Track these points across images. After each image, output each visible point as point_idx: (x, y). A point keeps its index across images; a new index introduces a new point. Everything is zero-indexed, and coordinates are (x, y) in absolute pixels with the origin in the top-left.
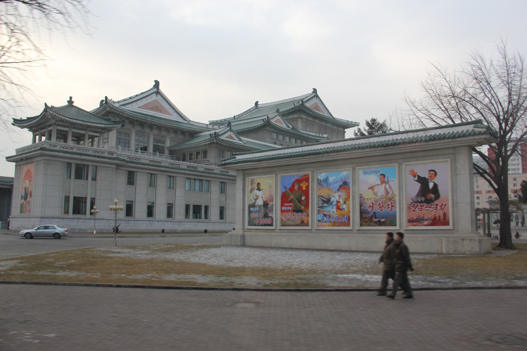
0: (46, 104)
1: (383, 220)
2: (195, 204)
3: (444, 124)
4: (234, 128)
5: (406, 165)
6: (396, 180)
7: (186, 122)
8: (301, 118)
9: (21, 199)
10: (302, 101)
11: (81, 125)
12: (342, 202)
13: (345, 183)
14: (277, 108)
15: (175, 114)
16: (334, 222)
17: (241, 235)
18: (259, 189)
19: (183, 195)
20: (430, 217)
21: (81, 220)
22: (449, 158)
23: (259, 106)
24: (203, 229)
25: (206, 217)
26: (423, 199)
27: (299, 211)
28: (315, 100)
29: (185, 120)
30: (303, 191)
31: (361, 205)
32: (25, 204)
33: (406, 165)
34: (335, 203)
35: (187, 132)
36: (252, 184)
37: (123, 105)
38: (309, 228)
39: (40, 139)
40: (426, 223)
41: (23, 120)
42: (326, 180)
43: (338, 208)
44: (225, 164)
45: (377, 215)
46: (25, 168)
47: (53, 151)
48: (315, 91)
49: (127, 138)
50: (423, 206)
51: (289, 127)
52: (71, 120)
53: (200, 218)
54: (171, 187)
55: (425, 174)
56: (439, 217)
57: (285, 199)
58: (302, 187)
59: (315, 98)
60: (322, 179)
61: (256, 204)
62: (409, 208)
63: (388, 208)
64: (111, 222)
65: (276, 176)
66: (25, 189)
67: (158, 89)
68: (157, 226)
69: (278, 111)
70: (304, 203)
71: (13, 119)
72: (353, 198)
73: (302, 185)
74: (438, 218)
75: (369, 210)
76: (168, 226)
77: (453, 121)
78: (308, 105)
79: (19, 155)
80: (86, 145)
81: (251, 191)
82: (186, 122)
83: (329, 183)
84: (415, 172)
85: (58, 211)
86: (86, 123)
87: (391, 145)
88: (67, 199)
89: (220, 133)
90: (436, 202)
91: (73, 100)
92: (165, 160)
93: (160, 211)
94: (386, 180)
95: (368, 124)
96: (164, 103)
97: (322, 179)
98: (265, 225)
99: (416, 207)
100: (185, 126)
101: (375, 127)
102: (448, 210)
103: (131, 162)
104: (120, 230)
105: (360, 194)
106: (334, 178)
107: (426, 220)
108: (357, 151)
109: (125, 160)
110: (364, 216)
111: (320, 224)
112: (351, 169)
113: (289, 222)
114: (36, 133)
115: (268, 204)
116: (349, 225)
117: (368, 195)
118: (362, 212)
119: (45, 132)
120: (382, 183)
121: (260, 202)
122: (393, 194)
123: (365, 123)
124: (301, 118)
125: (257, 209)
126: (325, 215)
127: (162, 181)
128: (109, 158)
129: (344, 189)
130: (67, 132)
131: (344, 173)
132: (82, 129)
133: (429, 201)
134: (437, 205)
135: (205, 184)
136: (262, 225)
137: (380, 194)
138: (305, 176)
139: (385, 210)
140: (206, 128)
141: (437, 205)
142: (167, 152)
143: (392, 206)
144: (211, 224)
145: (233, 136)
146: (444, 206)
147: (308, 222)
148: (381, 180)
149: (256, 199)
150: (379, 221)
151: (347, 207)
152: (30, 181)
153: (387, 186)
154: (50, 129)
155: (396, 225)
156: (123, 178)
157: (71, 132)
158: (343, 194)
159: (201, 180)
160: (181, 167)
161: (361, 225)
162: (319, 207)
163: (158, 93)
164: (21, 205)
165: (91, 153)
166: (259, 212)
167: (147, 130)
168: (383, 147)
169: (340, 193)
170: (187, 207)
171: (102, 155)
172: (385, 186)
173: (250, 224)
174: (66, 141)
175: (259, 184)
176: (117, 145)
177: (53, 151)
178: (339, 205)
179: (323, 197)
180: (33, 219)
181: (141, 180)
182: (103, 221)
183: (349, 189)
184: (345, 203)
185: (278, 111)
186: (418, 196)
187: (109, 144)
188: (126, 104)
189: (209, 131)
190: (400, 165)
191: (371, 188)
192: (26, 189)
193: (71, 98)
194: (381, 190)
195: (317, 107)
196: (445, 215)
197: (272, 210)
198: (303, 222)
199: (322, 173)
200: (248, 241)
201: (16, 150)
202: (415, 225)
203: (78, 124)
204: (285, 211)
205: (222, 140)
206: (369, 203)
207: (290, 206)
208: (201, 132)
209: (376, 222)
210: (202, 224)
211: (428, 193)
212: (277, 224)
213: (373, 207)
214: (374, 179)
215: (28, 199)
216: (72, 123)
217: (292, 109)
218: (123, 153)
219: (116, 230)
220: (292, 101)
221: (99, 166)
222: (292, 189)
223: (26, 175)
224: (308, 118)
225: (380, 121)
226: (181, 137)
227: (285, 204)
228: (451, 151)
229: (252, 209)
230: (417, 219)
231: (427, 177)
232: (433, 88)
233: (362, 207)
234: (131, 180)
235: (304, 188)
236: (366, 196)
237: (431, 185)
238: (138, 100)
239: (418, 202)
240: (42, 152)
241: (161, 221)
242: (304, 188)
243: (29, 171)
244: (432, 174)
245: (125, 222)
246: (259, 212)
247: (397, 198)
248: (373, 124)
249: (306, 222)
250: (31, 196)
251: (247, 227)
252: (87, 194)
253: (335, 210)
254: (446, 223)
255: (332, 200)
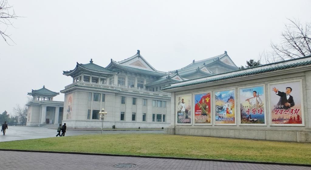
0: (77, 63)
1: (256, 120)
2: (158, 114)
3: (296, 57)
4: (180, 75)
5: (271, 85)
6: (264, 95)
7: (155, 71)
8: (218, 68)
9: (67, 112)
10: (218, 58)
11: (97, 73)
12: (230, 109)
13: (232, 98)
14: (204, 63)
15: (149, 67)
16: (226, 121)
17: (173, 129)
18: (183, 103)
19: (151, 109)
20: (288, 117)
21: (96, 122)
22: (301, 79)
23: (195, 63)
24: (161, 127)
25: (164, 121)
26: (283, 106)
27: (204, 114)
28: (226, 58)
29: (154, 70)
30: (207, 103)
31: (241, 111)
32: (68, 114)
33: (271, 85)
34: (226, 109)
35: (157, 77)
36: (179, 100)
37: (121, 63)
38: (211, 124)
39: (77, 81)
40: (285, 122)
41: (68, 72)
42: (220, 96)
43: (227, 112)
44: (164, 89)
45: (251, 116)
46: (69, 96)
47: (82, 86)
48: (226, 52)
49: (123, 80)
50: (282, 111)
51: (211, 73)
52: (91, 71)
53: (161, 121)
54: (145, 105)
55: (283, 90)
56: (294, 118)
57: (197, 108)
58: (206, 100)
59: (226, 56)
60: (218, 96)
61: (182, 111)
62: (272, 112)
63: (259, 112)
64: (112, 123)
65: (192, 94)
66: (69, 106)
67: (139, 54)
68: (136, 126)
69: (204, 64)
70: (208, 109)
71: (63, 71)
72: (236, 106)
73: (206, 99)
74: (293, 118)
75: (247, 113)
76: (143, 125)
77: (303, 54)
78: (222, 60)
79: (67, 89)
80: (100, 83)
81: (179, 104)
82: (155, 71)
83: (222, 97)
84: (277, 89)
85: (84, 118)
86: (99, 72)
87: (260, 72)
88: (89, 111)
89: (171, 77)
90: (292, 108)
91: (92, 61)
92: (142, 91)
93: (139, 117)
94: (257, 95)
95: (248, 63)
96: (143, 62)
97: (218, 96)
98: (186, 123)
99: (278, 111)
100: (155, 74)
101: (251, 64)
102: (301, 113)
103: (123, 92)
104: (116, 127)
105: (241, 104)
106: (225, 95)
107: (285, 120)
108: (238, 78)
109: (119, 91)
110: (243, 117)
111: (217, 122)
112: (235, 89)
113: (199, 121)
114: (75, 78)
115: (188, 111)
116: (234, 123)
117: (246, 104)
118: (242, 115)
119: (78, 77)
120: (254, 96)
121: (184, 110)
122: (262, 103)
123: (246, 63)
124: (218, 68)
125: (182, 114)
126: (220, 117)
127: (139, 102)
128: (111, 90)
129: (231, 101)
130: (89, 77)
131: (231, 92)
132: (97, 75)
133: (287, 108)
134: (292, 110)
135: (163, 103)
136: (185, 123)
137: (253, 104)
138: (208, 94)
139: (257, 113)
140: (165, 74)
141: (292, 110)
142: (144, 87)
143: (261, 111)
144: (137, 123)
145: (179, 78)
146: (297, 111)
147: (210, 121)
148: (254, 95)
149: (181, 108)
150: (253, 120)
151: (233, 112)
152: (71, 103)
153: (258, 98)
154: (80, 75)
155: (264, 123)
156: (119, 100)
157: (100, 77)
158: (230, 104)
159: (162, 101)
160: (150, 94)
161: (242, 123)
162: (216, 112)
163: (139, 56)
164: (67, 115)
165: (110, 88)
166: (183, 115)
167: (134, 76)
168: (257, 75)
169: (228, 103)
170: (154, 115)
171: (108, 88)
172: (257, 99)
173: (178, 122)
174: (89, 81)
175: (183, 99)
176: (118, 84)
177: (82, 86)
178: (228, 111)
179: (219, 106)
180: (72, 122)
181: (129, 101)
182: (108, 123)
183: (234, 101)
184: (232, 109)
185: (204, 64)
186: (279, 104)
187: (115, 83)
188: (122, 63)
189: (166, 76)
190: (266, 85)
191: (247, 100)
192: (69, 106)
193: (91, 59)
194: (254, 101)
195: (227, 61)
196: (298, 116)
197: (190, 114)
198: (207, 121)
199: (217, 92)
200: (177, 132)
201: (65, 87)
202: (277, 123)
203: (95, 73)
204: (197, 115)
205: (173, 80)
206: (246, 109)
207: (200, 112)
208: (163, 76)
209: (251, 121)
210: (162, 124)
211: (286, 102)
212: (193, 123)
213: (249, 111)
214: (249, 95)
215: (70, 111)
216: (92, 72)
217: (213, 63)
218: (119, 87)
219: (114, 127)
220: (213, 59)
221: (106, 94)
222: (201, 102)
223: (69, 99)
224: (222, 67)
225: (256, 61)
226: (152, 79)
227: (197, 111)
228: (303, 74)
229: (179, 114)
230: (278, 119)
231: (285, 92)
232: (289, 34)
233: (242, 112)
234: (123, 102)
235: (208, 101)
236: (244, 105)
237: (288, 97)
238: (129, 61)
239: (279, 108)
240: (76, 87)
241: (139, 123)
242: (208, 101)
243: (70, 97)
244: (289, 90)
245: (120, 123)
246: (183, 115)
247: (264, 106)
248: (251, 63)
249: (209, 121)
250: (71, 110)
251: (177, 124)
252: (100, 109)
253: (225, 114)
254: (300, 122)
255: (224, 108)
